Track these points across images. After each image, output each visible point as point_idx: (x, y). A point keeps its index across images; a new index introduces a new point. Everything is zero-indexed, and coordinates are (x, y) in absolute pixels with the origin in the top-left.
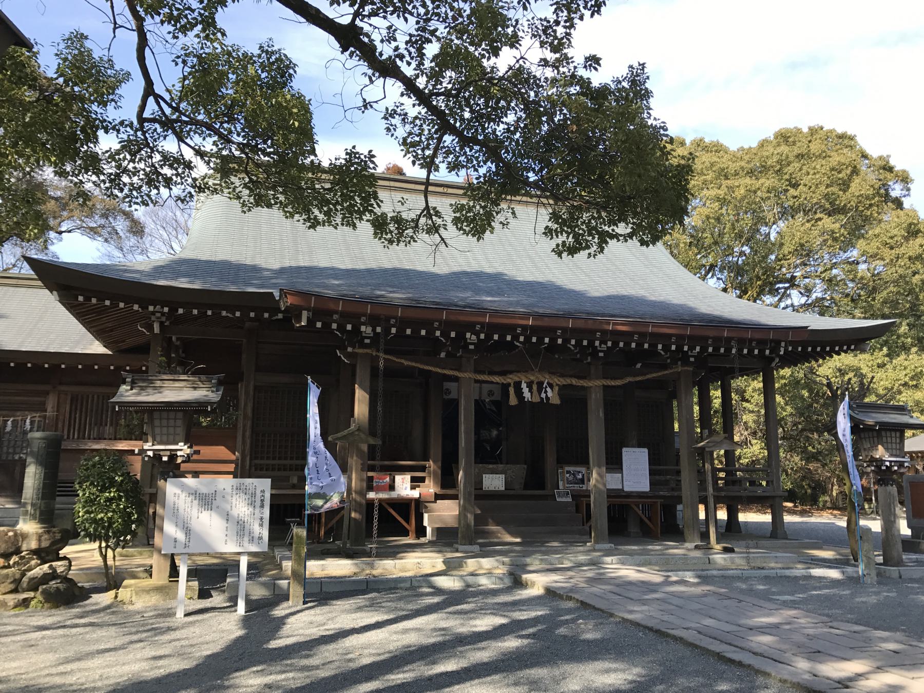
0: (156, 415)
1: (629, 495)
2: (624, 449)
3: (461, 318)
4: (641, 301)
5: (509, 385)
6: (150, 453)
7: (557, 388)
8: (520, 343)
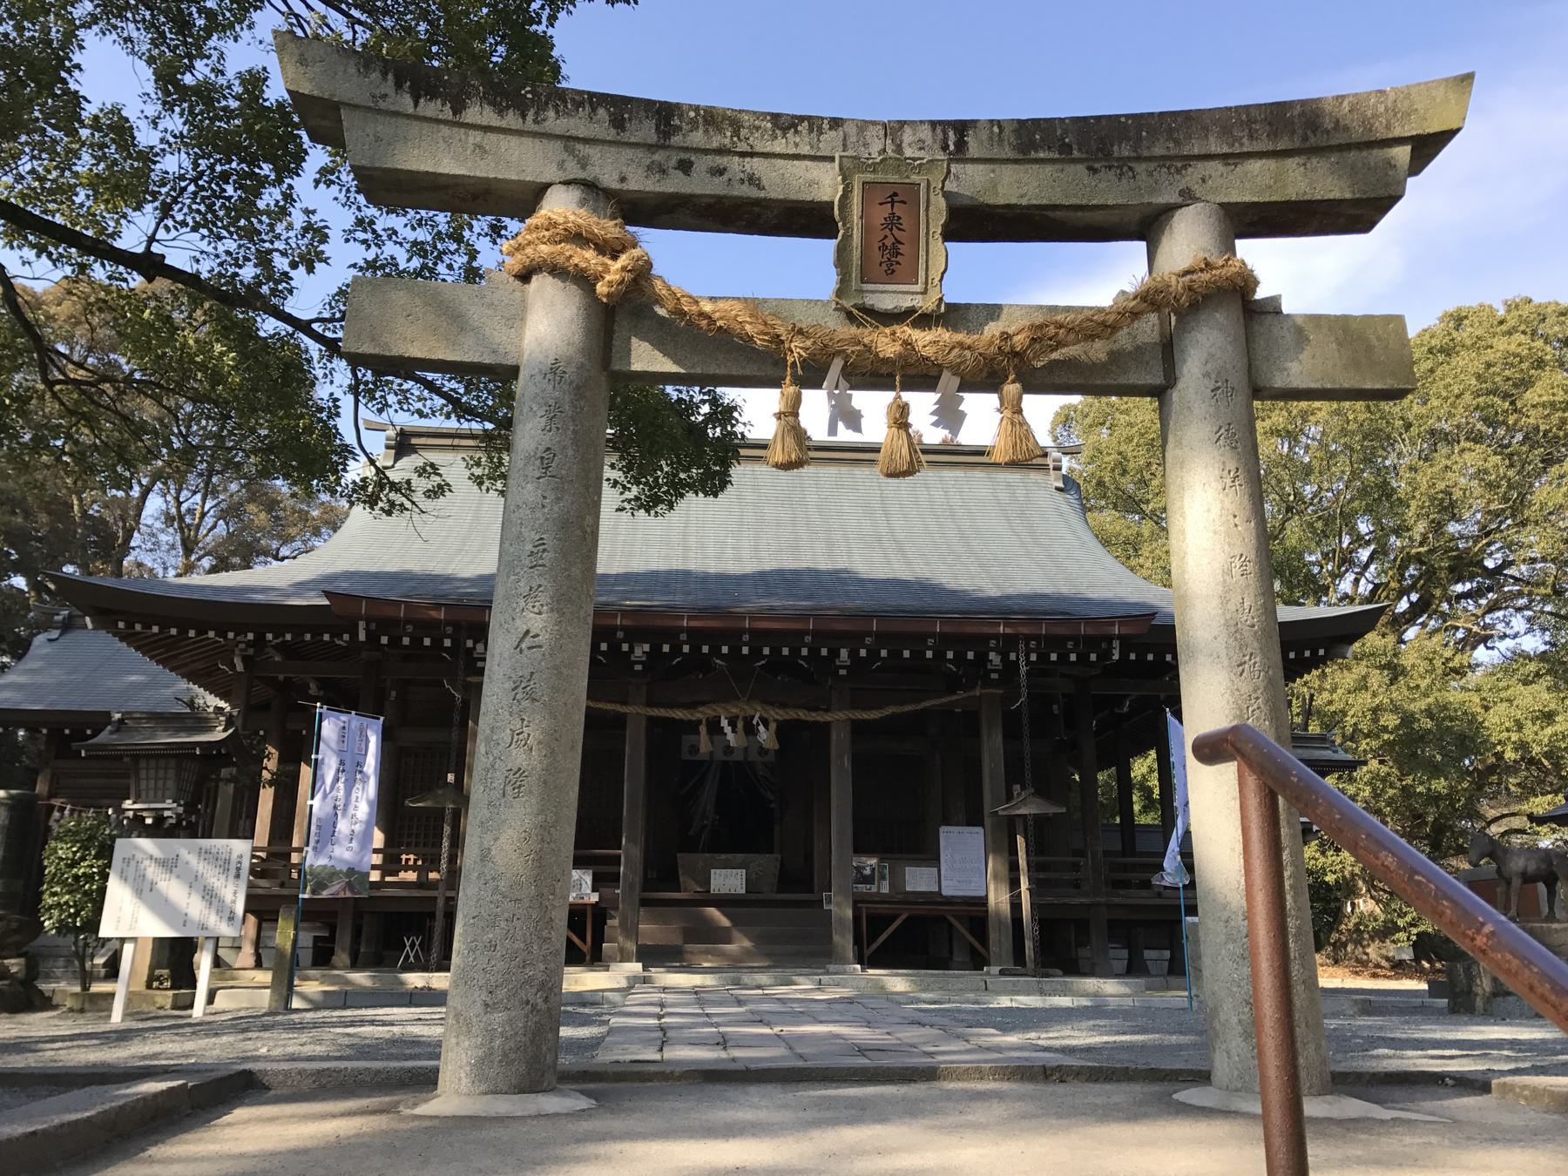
0: (143, 764)
1: (950, 901)
2: (943, 829)
3: (659, 623)
4: (840, 579)
5: (700, 722)
6: (130, 814)
7: (773, 726)
8: (804, 658)
